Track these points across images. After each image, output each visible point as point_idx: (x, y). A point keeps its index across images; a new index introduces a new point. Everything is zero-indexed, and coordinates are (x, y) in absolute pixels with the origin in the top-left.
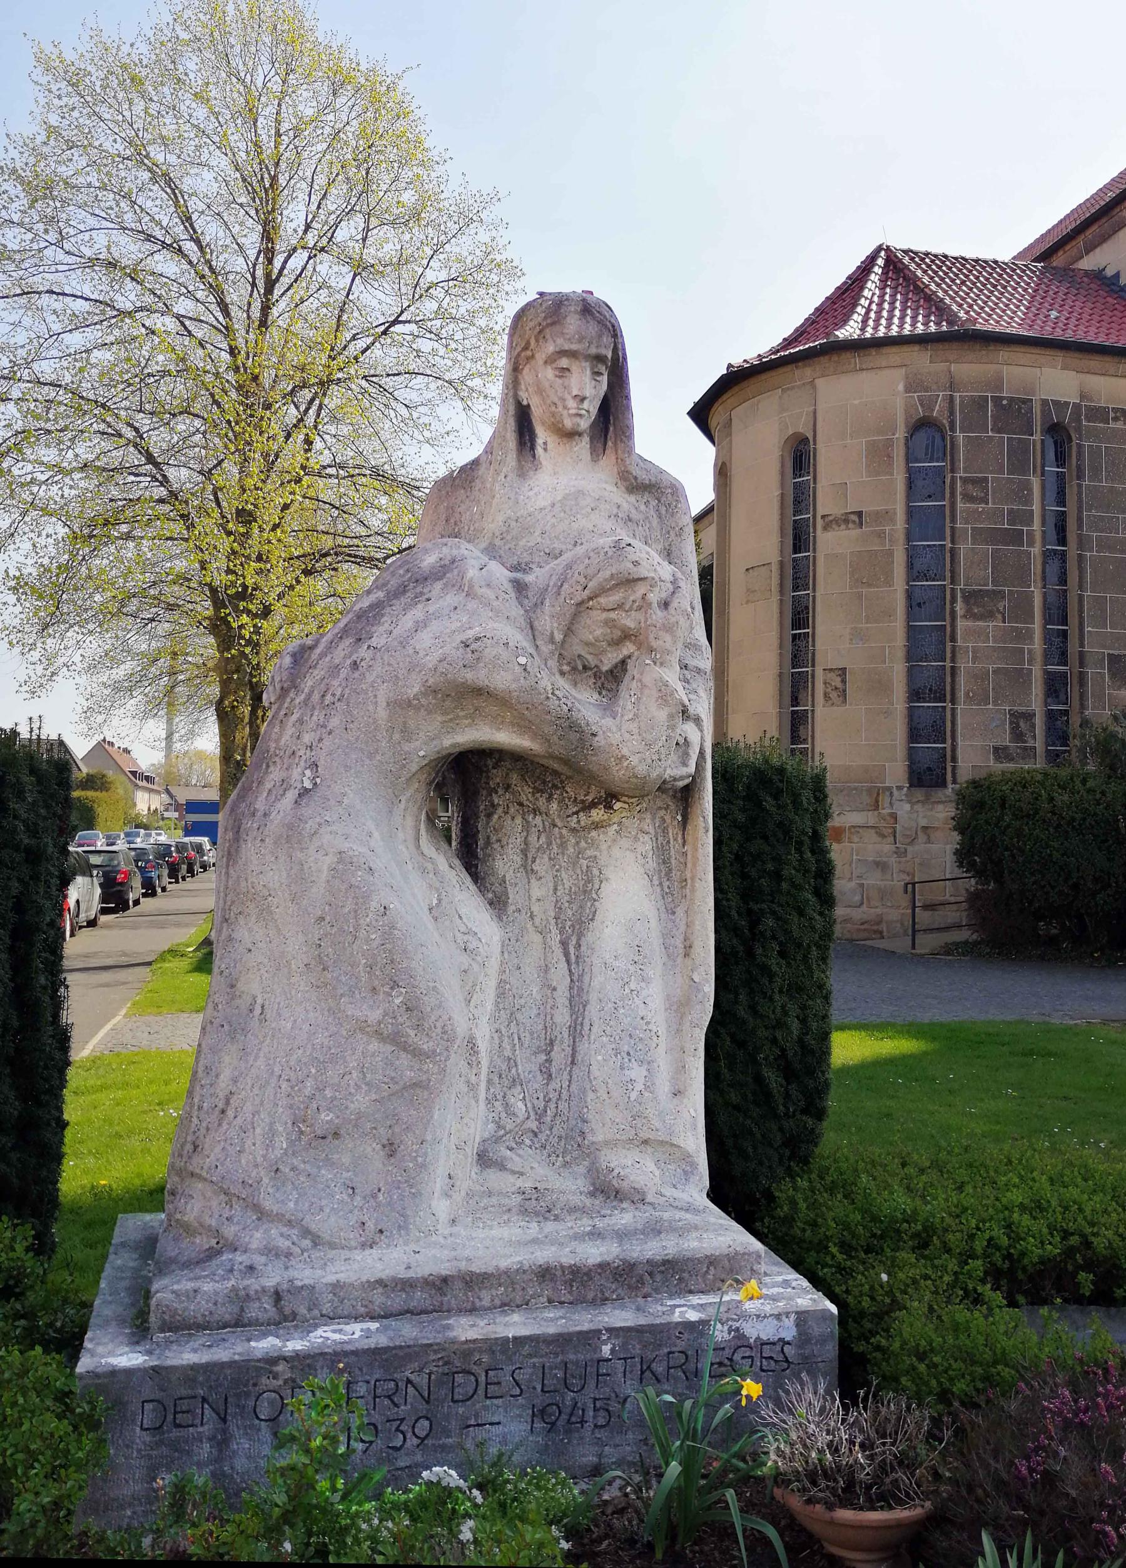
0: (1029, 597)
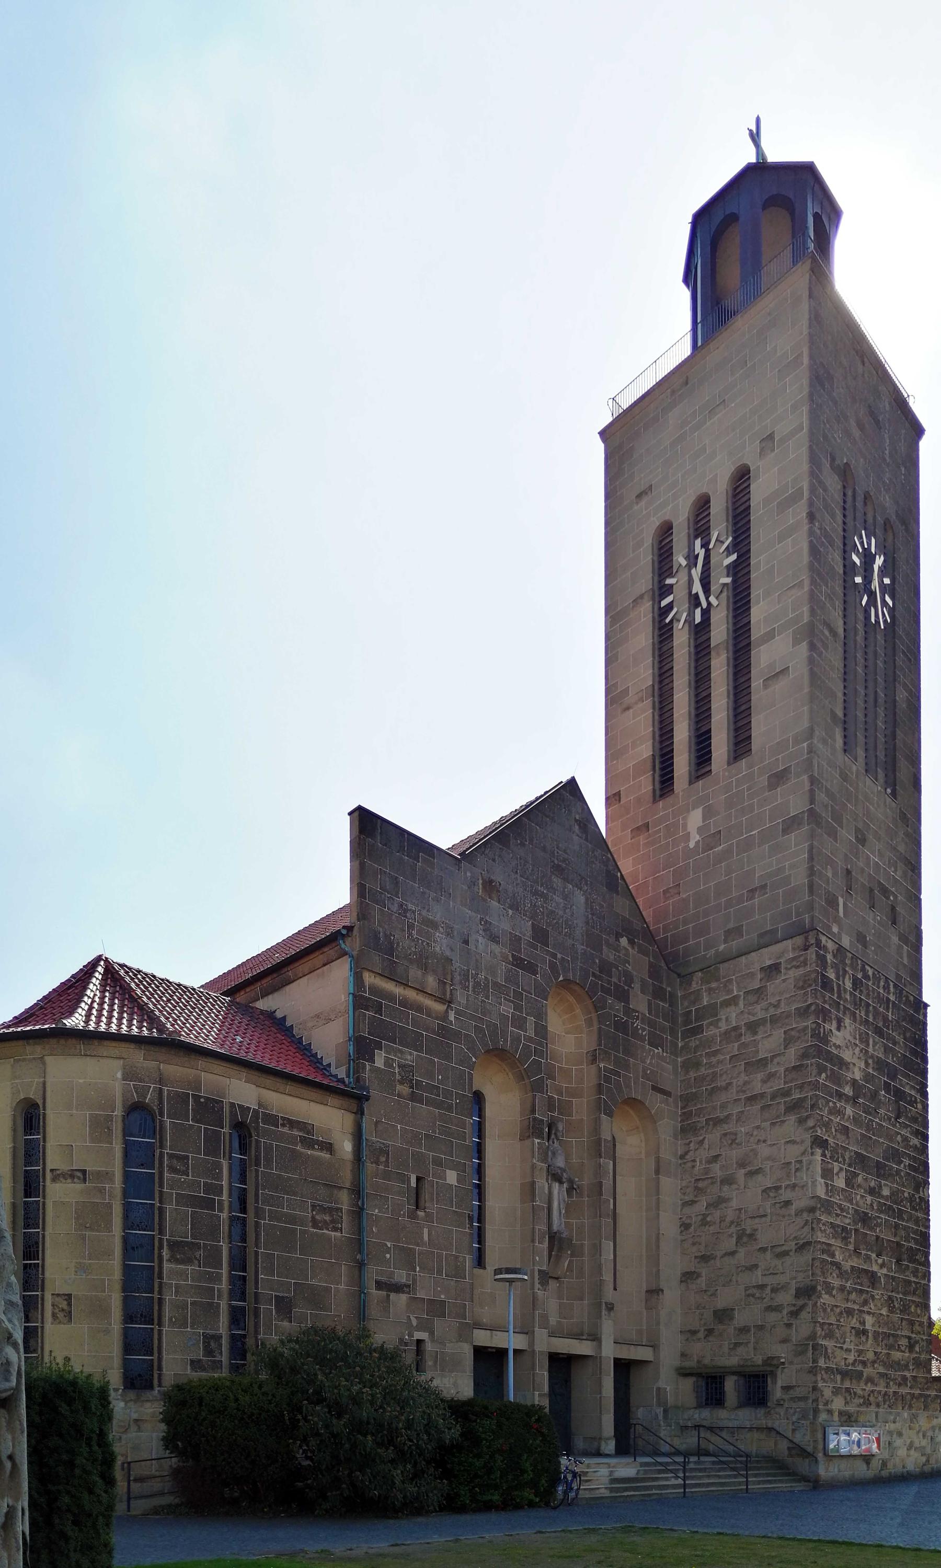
0: (219, 1250)
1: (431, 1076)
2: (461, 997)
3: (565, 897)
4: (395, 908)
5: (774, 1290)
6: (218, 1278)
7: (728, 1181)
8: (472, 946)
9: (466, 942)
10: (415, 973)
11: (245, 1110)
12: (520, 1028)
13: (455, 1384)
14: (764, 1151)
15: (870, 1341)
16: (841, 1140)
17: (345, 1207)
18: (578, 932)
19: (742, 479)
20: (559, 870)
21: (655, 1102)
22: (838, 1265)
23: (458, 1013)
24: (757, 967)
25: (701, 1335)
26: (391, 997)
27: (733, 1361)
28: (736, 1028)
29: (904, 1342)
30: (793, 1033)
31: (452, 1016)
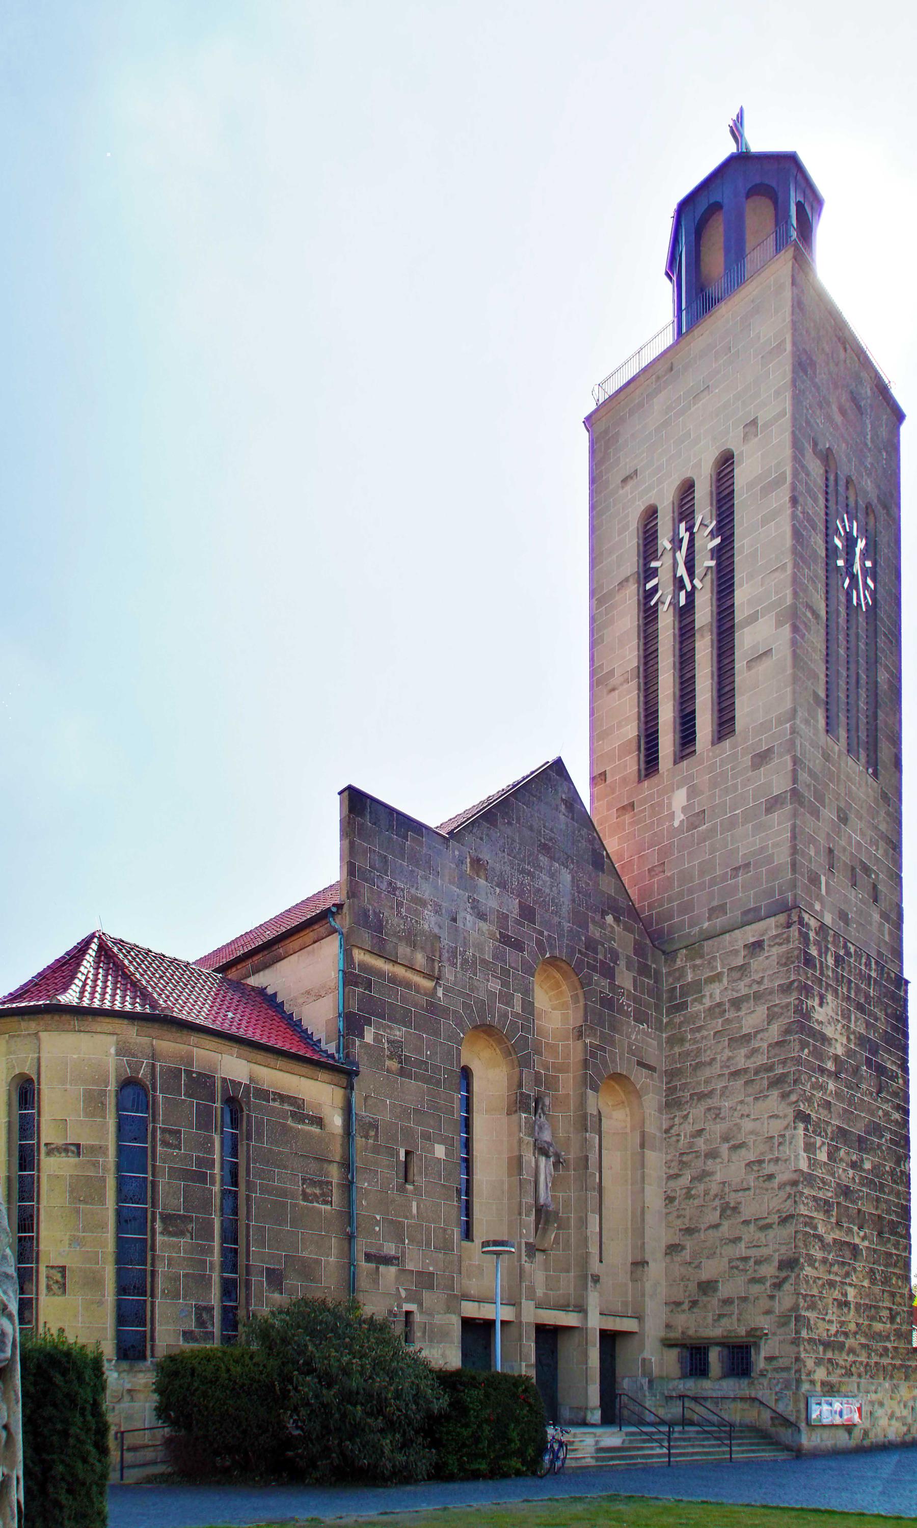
0: (211, 1223)
1: (419, 1051)
2: (449, 974)
3: (552, 876)
4: (384, 886)
5: (758, 1262)
6: (210, 1251)
7: (713, 1154)
8: (460, 924)
9: (454, 920)
10: (403, 950)
11: (236, 1084)
12: (507, 1004)
13: (443, 1355)
14: (747, 1125)
15: (852, 1312)
16: (823, 1114)
17: (335, 1181)
18: (564, 910)
19: (726, 464)
20: (545, 848)
21: (640, 1077)
22: (820, 1238)
23: (446, 989)
24: (741, 944)
25: (685, 1306)
26: (380, 974)
27: (716, 1332)
28: (719, 1005)
29: (885, 1313)
30: (776, 1009)
31: (440, 992)
